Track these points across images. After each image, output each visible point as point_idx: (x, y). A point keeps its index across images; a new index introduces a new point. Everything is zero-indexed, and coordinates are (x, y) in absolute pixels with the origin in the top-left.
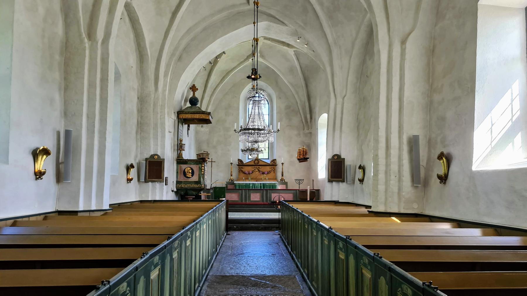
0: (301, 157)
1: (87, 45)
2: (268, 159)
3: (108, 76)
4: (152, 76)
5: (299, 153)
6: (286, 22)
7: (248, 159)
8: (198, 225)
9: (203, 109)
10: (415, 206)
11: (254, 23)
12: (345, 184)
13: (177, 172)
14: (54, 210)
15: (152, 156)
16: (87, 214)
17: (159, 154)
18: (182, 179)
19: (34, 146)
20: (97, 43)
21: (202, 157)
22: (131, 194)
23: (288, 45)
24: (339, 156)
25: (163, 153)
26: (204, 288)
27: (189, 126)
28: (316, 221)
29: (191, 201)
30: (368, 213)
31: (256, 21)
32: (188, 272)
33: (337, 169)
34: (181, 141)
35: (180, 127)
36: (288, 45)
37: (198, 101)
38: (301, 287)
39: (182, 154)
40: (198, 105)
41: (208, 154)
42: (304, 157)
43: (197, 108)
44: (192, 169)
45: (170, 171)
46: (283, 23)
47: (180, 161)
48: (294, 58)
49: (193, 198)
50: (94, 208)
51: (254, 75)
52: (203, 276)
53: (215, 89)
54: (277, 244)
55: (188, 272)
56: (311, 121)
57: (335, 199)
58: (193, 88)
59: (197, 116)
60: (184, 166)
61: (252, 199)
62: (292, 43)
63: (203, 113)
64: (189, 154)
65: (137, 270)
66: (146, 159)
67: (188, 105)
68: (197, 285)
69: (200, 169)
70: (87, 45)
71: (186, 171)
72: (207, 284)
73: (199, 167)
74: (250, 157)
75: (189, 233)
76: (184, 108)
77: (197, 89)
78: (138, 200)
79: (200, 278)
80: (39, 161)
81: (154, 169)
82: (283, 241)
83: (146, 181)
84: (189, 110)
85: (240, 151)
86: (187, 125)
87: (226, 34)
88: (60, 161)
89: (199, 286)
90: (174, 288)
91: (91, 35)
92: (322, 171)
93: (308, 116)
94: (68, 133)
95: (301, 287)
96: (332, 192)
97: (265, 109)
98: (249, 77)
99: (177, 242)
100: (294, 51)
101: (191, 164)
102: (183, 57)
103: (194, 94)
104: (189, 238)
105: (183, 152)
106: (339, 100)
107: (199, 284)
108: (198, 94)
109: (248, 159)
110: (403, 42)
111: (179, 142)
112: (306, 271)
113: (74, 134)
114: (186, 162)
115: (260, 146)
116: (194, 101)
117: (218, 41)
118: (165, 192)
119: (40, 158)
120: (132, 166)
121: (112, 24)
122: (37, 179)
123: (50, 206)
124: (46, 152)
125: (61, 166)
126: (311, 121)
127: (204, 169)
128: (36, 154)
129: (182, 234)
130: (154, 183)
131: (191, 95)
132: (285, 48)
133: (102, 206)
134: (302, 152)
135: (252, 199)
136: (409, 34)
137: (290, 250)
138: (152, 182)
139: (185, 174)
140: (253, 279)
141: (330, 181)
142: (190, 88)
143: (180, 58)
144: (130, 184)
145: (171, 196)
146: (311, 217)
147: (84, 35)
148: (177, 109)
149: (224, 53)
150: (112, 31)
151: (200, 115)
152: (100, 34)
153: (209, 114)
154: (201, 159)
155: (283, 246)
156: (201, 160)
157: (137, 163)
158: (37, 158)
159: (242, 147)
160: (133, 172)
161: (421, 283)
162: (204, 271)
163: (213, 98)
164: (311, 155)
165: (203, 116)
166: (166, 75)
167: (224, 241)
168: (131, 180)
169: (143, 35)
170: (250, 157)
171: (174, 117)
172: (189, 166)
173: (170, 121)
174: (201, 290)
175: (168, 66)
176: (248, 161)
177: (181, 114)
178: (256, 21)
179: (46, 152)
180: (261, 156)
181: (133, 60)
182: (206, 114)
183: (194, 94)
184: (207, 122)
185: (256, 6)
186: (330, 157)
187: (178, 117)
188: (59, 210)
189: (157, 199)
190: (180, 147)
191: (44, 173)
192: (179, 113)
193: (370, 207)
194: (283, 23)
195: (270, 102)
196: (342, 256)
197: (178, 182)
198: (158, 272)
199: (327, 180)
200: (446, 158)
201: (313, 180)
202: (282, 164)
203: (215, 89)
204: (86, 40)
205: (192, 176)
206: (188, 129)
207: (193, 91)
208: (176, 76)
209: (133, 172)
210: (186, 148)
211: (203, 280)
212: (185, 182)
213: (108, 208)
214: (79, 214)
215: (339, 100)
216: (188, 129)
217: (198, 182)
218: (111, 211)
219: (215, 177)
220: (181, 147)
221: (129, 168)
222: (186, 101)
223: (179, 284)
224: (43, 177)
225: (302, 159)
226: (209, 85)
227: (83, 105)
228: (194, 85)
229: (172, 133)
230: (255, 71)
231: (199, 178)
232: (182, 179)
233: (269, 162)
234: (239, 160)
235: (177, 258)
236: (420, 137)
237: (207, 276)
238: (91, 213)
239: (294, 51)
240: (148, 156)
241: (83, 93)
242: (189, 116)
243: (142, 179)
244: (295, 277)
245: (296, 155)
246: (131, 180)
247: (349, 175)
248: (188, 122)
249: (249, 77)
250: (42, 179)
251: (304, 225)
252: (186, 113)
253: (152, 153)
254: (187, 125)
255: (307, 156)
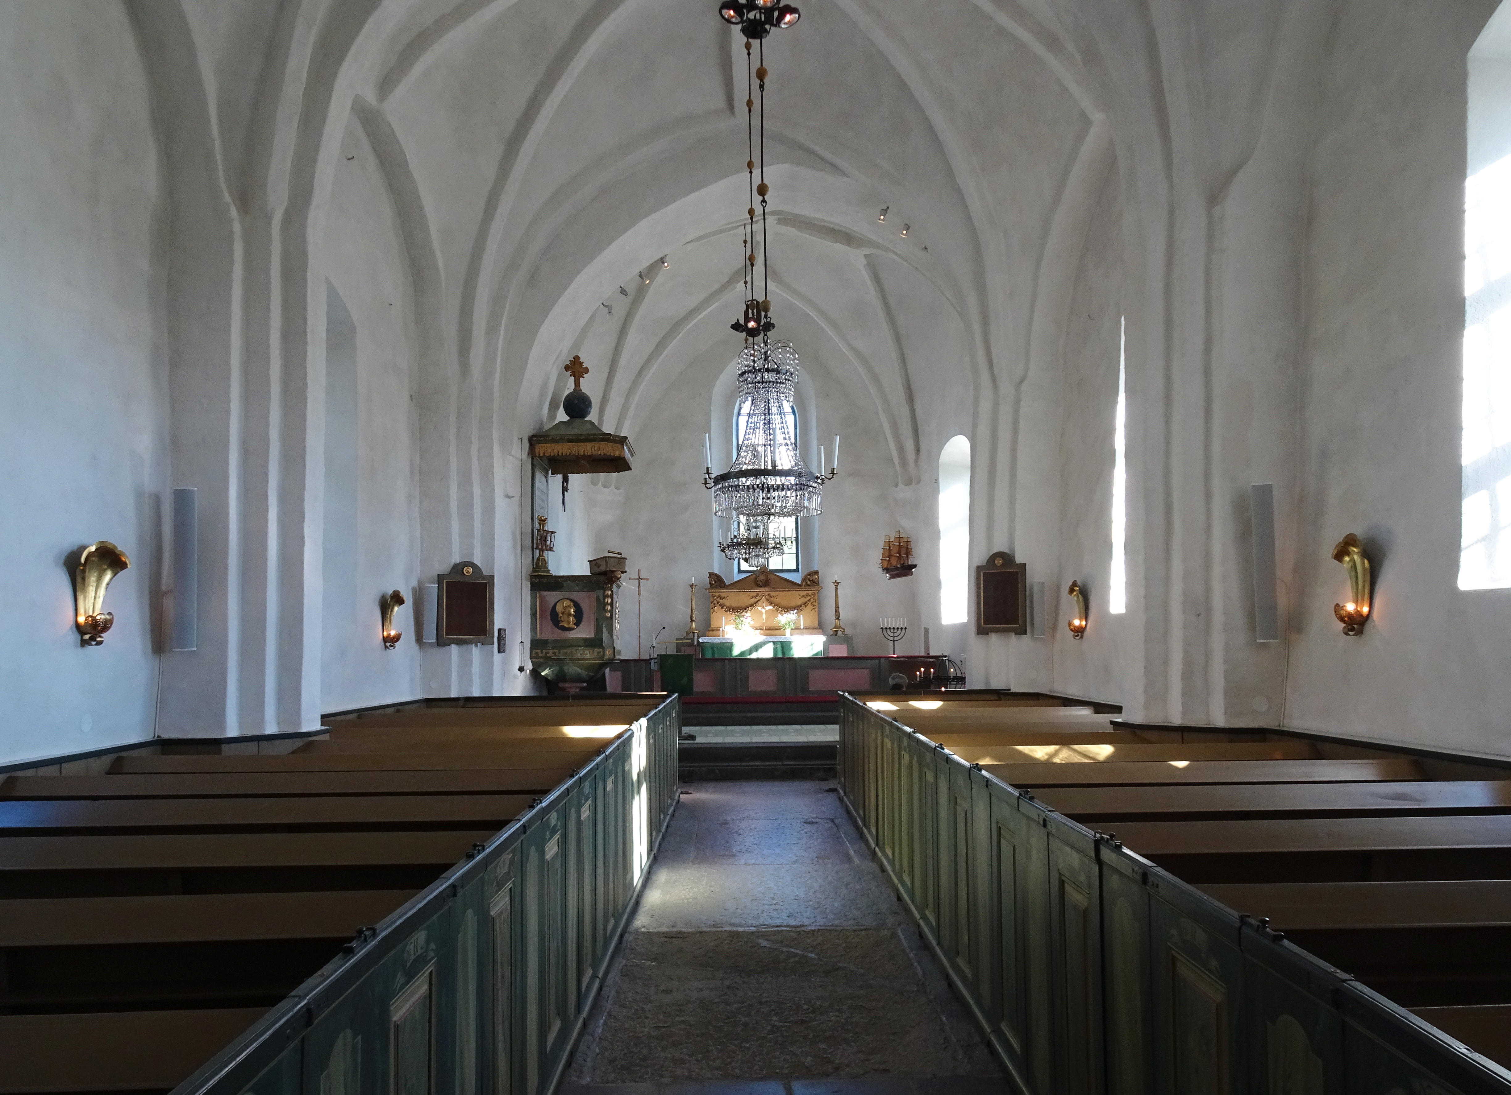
0: (894, 562)
1: (237, 228)
2: (797, 570)
3: (305, 323)
4: (450, 330)
5: (888, 553)
6: (842, 163)
7: (740, 571)
8: (587, 784)
9: (608, 428)
10: (1260, 704)
11: (750, 165)
12: (1026, 639)
13: (534, 615)
14: (149, 737)
15: (458, 568)
16: (251, 749)
17: (477, 561)
18: (549, 633)
19: (68, 542)
20: (269, 220)
21: (603, 568)
22: (400, 679)
23: (848, 238)
24: (1006, 558)
25: (490, 557)
26: (610, 980)
27: (565, 480)
28: (933, 744)
29: (575, 697)
30: (1110, 729)
31: (756, 160)
32: (554, 945)
33: (1002, 594)
34: (543, 521)
35: (537, 483)
36: (848, 238)
37: (590, 405)
38: (919, 970)
39: (545, 563)
40: (593, 416)
41: (621, 560)
42: (900, 561)
43: (589, 426)
44: (572, 600)
45: (510, 610)
46: (834, 166)
47: (541, 581)
48: (866, 276)
49: (582, 689)
50: (271, 729)
51: (755, 322)
52: (607, 940)
53: (640, 374)
54: (832, 820)
55: (554, 945)
56: (917, 460)
57: (997, 684)
58: (576, 368)
59: (587, 449)
60: (552, 597)
61: (752, 688)
62: (860, 226)
63: (606, 438)
64: (571, 559)
65: (309, 1023)
66: (440, 578)
67: (562, 416)
68: (589, 972)
69: (601, 605)
70: (237, 228)
71: (559, 608)
72: (620, 963)
73: (598, 599)
74: (744, 566)
75: (553, 818)
76: (547, 427)
77: (587, 370)
78: (419, 697)
79: (599, 952)
80: (91, 590)
81: (462, 606)
82: (848, 812)
83: (441, 642)
84: (563, 431)
85: (716, 550)
86: (559, 477)
87: (666, 204)
88: (164, 587)
89: (594, 976)
90: (499, 1019)
91: (248, 195)
92: (954, 602)
93: (909, 446)
94: (182, 499)
95: (919, 970)
96: (999, 662)
97: (786, 422)
98: (736, 327)
99: (507, 857)
100: (865, 256)
101: (571, 590)
102: (544, 273)
103: (577, 384)
104: (553, 832)
105: (549, 556)
106: (1007, 389)
107: (595, 966)
108: (590, 386)
109: (740, 571)
110: (1214, 198)
111: (537, 526)
112: (861, 813)
113: (199, 503)
114: (558, 583)
115: (814, 497)
116: (577, 406)
117: (644, 225)
118: (506, 672)
119: (92, 579)
120: (397, 599)
121: (314, 161)
122: (84, 643)
123: (126, 726)
124: (110, 558)
125: (169, 603)
126: (917, 460)
127: (612, 604)
128: (76, 568)
129: (524, 828)
130: (465, 647)
131: (569, 387)
132: (839, 247)
133: (299, 724)
134: (894, 551)
135: (752, 688)
136: (1234, 172)
137: (873, 845)
138: (460, 643)
139: (555, 619)
140: (765, 944)
141: (981, 631)
142: (567, 368)
143: (533, 279)
144: (391, 651)
145: (517, 686)
146: (947, 751)
147: (227, 197)
148: (529, 429)
149: (662, 260)
150: (316, 184)
151: (597, 444)
152: (277, 194)
153: (623, 440)
154: (605, 573)
155: (850, 828)
156: (605, 574)
157: (414, 590)
158: (84, 579)
159: (718, 537)
160: (402, 617)
161: (1235, 914)
162: (612, 922)
163: (636, 399)
164: (919, 557)
165: (608, 449)
166: (492, 328)
167: (673, 815)
168: (397, 638)
169: (421, 208)
170: (744, 566)
171: (519, 452)
172: (567, 594)
173: (508, 464)
174: (600, 988)
175: (498, 300)
176: (737, 577)
177: (539, 442)
178: (756, 160)
179: (110, 558)
180: (776, 563)
181: (392, 282)
182: (614, 441)
183: (577, 384)
184: (619, 464)
185: (756, 83)
186: (981, 559)
187: (532, 452)
188: (166, 736)
189: (476, 693)
190: (540, 539)
191: (106, 626)
192: (535, 440)
193: (1118, 709)
194: (835, 168)
195: (800, 410)
196: (930, 777)
197: (537, 645)
198: (426, 987)
199: (973, 629)
200: (1365, 554)
201: (927, 631)
202: (837, 583)
203: (640, 374)
204: (234, 212)
205: (577, 624)
206: (565, 489)
207: (573, 374)
208: (526, 330)
209: (402, 617)
210: (559, 542)
211: (610, 952)
212: (556, 641)
213: (317, 726)
214: (225, 748)
215: (1007, 389)
216: (565, 489)
217: (595, 643)
218: (326, 737)
219: (637, 626)
220: (544, 539)
221: (389, 603)
222: (553, 407)
223: (518, 1000)
224: (105, 636)
225: (896, 568)
226: (623, 361)
227: (228, 412)
228: (576, 358)
229: (516, 499)
230: (757, 309)
231: (599, 630)
232: (549, 633)
233: (797, 578)
234: (711, 574)
235: (506, 915)
236: (1275, 492)
237: (622, 936)
238: (262, 743)
239: (865, 256)
240: (442, 566)
241: (227, 378)
242: (563, 449)
243: (430, 635)
244: (894, 934)
245: (876, 556)
246: (397, 638)
247: (1040, 612)
248: (563, 466)
249: (736, 327)
250: (99, 643)
251: (922, 776)
252: (554, 441)
253: (456, 559)
254: (559, 477)
255: (911, 561)
